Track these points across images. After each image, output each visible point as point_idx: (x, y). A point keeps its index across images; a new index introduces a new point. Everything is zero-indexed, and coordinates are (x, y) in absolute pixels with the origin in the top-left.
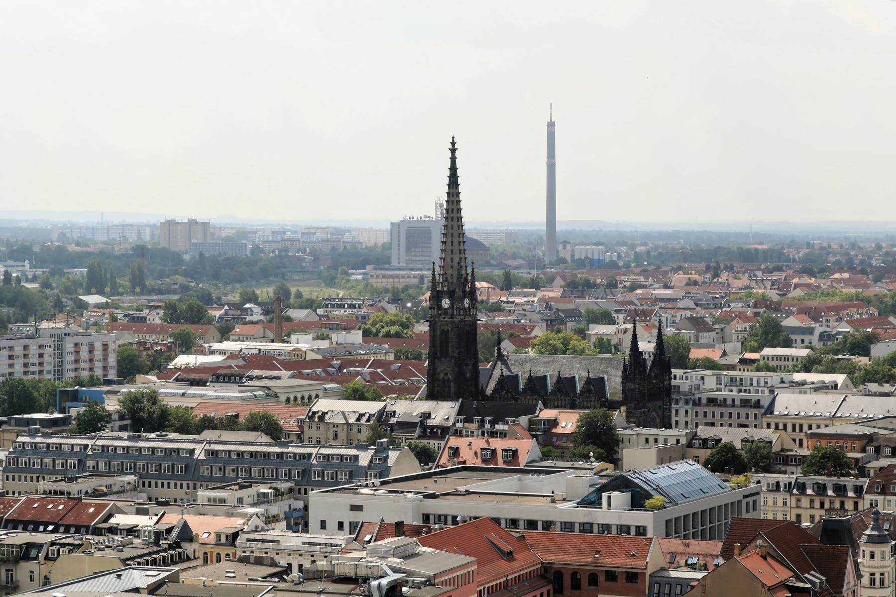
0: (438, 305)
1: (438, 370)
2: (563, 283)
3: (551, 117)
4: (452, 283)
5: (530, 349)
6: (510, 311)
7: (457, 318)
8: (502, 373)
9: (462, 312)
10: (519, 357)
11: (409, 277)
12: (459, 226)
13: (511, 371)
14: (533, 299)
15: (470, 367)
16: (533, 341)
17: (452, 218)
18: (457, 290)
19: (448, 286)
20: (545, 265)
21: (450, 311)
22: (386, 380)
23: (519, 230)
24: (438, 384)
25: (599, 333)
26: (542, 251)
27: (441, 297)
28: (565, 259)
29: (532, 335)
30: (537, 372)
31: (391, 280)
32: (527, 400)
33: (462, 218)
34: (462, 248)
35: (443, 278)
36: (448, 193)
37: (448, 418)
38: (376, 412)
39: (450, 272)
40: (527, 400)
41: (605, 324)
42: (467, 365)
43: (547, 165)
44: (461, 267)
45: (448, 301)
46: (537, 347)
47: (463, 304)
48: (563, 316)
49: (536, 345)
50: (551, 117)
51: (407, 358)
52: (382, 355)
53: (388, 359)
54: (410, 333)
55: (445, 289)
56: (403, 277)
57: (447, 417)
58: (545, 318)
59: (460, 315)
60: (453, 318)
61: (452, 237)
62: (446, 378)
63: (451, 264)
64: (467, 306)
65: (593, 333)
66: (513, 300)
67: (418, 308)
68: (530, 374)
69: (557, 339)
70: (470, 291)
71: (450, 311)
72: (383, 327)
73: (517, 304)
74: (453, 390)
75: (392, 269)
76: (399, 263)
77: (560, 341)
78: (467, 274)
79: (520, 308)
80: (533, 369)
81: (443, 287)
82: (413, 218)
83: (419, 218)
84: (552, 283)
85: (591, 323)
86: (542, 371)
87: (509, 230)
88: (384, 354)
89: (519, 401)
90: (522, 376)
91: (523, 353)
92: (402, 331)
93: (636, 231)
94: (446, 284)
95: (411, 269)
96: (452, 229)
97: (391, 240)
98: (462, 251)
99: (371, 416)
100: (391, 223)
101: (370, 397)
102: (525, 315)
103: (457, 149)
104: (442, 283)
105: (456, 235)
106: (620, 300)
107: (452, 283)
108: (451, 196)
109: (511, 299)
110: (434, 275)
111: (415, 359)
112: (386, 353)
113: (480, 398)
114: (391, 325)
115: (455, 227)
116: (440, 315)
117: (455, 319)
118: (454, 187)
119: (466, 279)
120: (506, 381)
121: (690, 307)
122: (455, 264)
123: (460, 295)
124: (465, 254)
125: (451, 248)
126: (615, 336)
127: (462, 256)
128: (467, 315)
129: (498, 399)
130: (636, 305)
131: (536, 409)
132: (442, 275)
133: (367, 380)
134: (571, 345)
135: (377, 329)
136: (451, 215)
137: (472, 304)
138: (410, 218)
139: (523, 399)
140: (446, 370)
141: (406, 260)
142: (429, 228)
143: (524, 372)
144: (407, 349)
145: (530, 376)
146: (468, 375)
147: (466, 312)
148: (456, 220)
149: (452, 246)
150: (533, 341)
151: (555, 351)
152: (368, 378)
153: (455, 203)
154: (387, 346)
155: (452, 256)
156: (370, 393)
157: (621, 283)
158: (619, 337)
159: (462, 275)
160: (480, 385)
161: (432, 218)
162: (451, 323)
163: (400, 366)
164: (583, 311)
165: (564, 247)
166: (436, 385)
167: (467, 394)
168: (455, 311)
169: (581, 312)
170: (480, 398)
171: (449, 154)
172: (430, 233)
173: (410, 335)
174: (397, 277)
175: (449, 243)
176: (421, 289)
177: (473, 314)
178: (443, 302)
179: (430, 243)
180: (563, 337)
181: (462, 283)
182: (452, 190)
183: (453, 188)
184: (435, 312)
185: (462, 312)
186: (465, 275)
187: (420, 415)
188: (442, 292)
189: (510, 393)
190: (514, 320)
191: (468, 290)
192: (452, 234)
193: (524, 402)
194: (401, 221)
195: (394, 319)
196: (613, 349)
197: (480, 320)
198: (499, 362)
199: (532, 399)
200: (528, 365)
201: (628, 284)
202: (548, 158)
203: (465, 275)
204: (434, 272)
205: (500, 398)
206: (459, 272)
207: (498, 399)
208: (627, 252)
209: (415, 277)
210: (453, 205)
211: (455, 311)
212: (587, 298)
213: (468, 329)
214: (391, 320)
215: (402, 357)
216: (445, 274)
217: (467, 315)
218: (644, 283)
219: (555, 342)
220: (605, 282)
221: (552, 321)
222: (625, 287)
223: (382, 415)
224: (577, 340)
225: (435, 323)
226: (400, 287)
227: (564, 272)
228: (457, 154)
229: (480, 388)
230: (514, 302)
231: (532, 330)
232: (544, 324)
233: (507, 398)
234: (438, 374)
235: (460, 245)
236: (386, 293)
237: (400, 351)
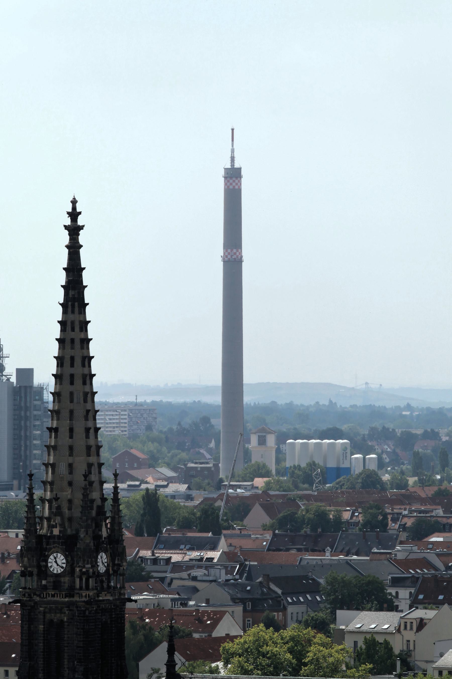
0: (39, 567)
2: (267, 520)
3: (233, 159)
4: (70, 519)
5: (220, 664)
7: (81, 596)
9: (91, 582)
16: (228, 645)
17: (72, 376)
19: (62, 525)
20: (221, 481)
21: (66, 579)
23: (153, 402)
25: (364, 629)
27: (46, 550)
28: (264, 466)
29: (219, 632)
34: (92, 442)
39: (67, 494)
41: (370, 610)
43: (224, 262)
44: (91, 483)
45: (61, 559)
47: (95, 565)
48: (279, 591)
49: (233, 655)
50: (233, 159)
55: (56, 531)
58: (239, 596)
59: (87, 588)
60: (73, 596)
61: (71, 419)
64: (102, 569)
65: (351, 627)
70: (109, 537)
73: (178, 567)
77: (286, 647)
78: (104, 500)
79: (184, 575)
81: (51, 527)
85: (342, 608)
93: (408, 407)
96: (72, 401)
98: (93, 449)
102: (195, 590)
103: (82, 227)
104: (49, 519)
105: (79, 413)
106: (400, 556)
107: (70, 519)
108: (69, 328)
109: (162, 554)
115: (79, 397)
116: (45, 588)
117: (76, 598)
118: (77, 309)
119: (101, 511)
122: (78, 478)
126: (398, 636)
127: (92, 459)
128: (102, 589)
130: (436, 569)
132: (50, 501)
134: (310, 654)
136: (68, 370)
137: (114, 565)
147: (102, 582)
148: (81, 382)
149: (71, 437)
153: (77, 344)
155: (70, 460)
157: (394, 520)
158: (406, 638)
159: (92, 501)
162: (69, 605)
164: (322, 581)
165: (262, 441)
168: (78, 581)
169: (319, 584)
171: (65, 238)
177: (115, 588)
180: (292, 639)
182: (71, 317)
183: (73, 312)
184: (32, 583)
185: (91, 582)
186: (99, 502)
188: (49, 538)
190: (173, 600)
191: (104, 533)
192: (71, 412)
196: (398, 664)
201: (409, 522)
203: (99, 502)
206: (85, 496)
208: (394, 452)
210: (72, 348)
211: (78, 581)
212: (328, 554)
216: (57, 499)
217: (102, 588)
218: (445, 521)
220: (361, 518)
221: (254, 602)
222: (404, 527)
224: (323, 645)
227: (269, 495)
228: (83, 238)
232: (239, 609)
235: (87, 437)
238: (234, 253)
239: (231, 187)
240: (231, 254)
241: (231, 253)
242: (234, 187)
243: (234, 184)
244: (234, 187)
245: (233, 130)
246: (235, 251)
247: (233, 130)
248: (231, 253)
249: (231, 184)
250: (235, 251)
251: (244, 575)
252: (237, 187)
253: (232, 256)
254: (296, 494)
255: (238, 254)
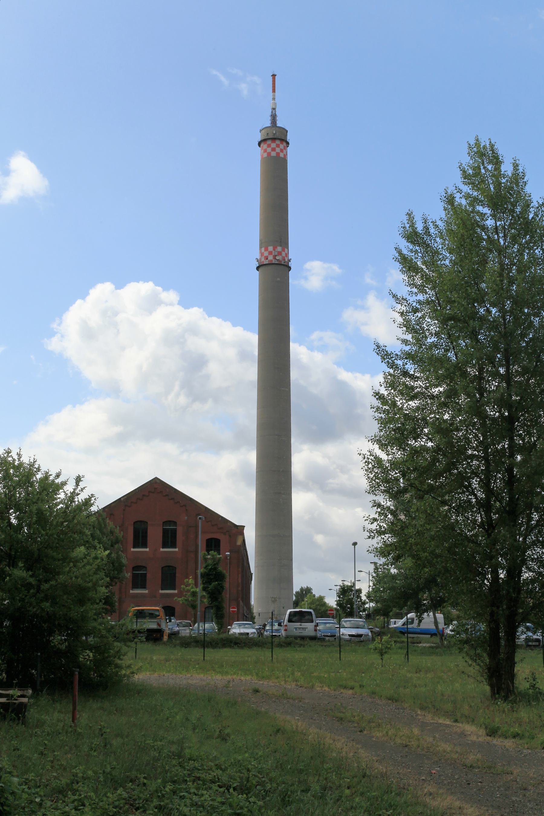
3: (274, 118)
238: (275, 148)
239: (273, 154)
240: (273, 254)
241: (273, 251)
242: (278, 154)
243: (278, 150)
244: (278, 154)
245: (274, 76)
246: (279, 249)
247: (274, 76)
248: (273, 251)
251: (132, 593)
252: (282, 155)
253: (275, 257)
254: (227, 673)
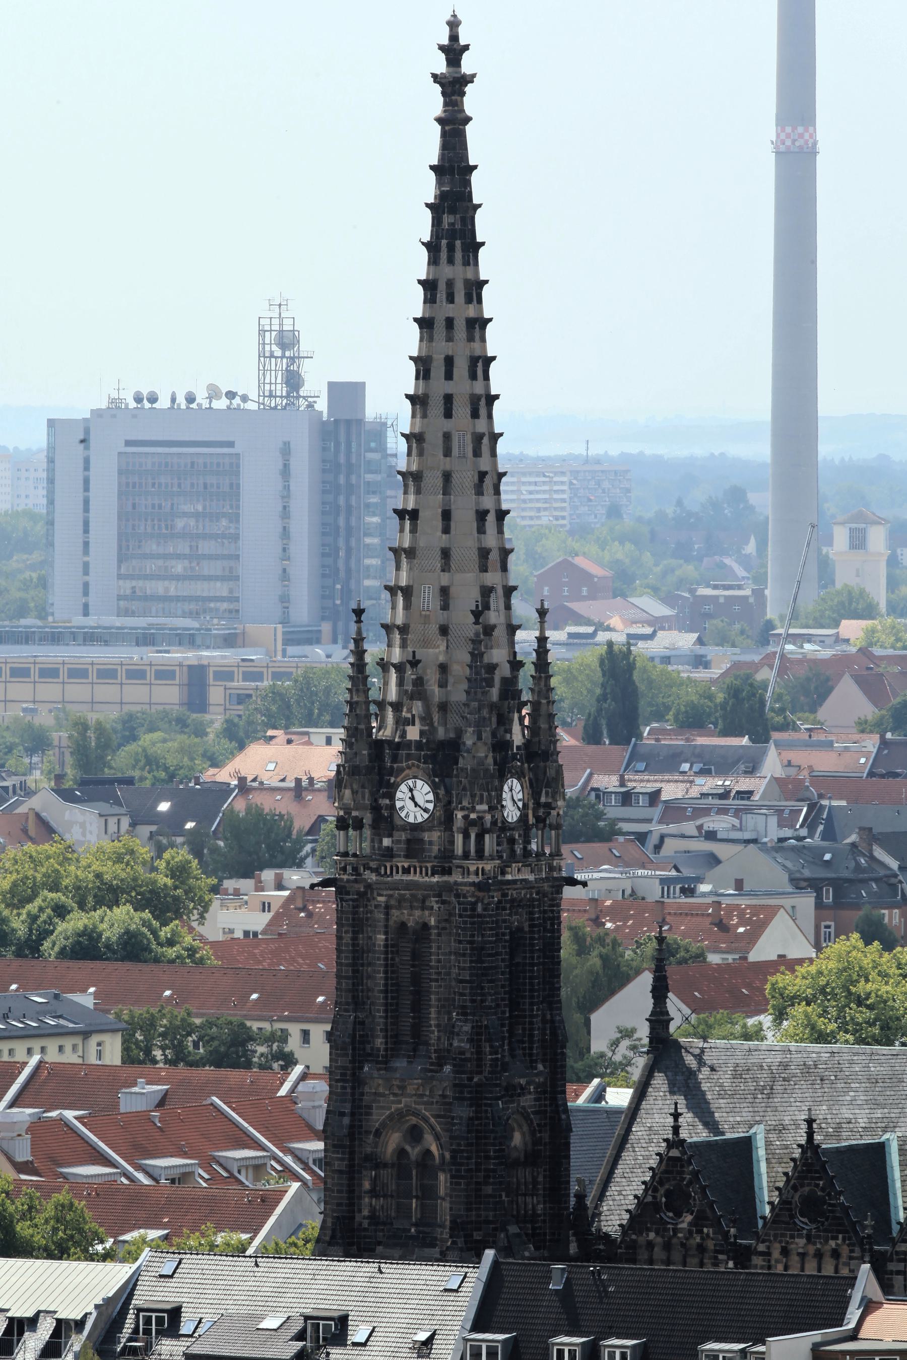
0: (376, 809)
1: (378, 1117)
2: (868, 710)
4: (444, 707)
5: (766, 1020)
6: (642, 837)
7: (466, 872)
8: (676, 1129)
10: (754, 1059)
11: (136, 674)
12: (478, 439)
13: (711, 1125)
14: (744, 784)
15: (527, 1101)
16: (782, 979)
17: (448, 399)
18: (469, 740)
19: (426, 719)
20: (770, 625)
21: (434, 837)
22: (107, 1161)
24: (374, 1181)
26: (745, 562)
27: (391, 772)
30: (838, 1128)
31: (50, 690)
32: (795, 1260)
33: (491, 399)
34: (490, 540)
35: (401, 683)
36: (429, 285)
37: (428, 1342)
38: (90, 1308)
39: (435, 653)
40: (795, 1260)
42: (512, 1092)
44: (489, 630)
45: (424, 792)
46: (799, 1010)
47: (496, 805)
49: (794, 999)
51: (179, 1057)
52: (68, 1043)
53: (93, 1060)
54: (188, 940)
56: (107, 674)
57: (423, 1336)
58: (807, 873)
59: (480, 855)
60: (449, 873)
61: (446, 491)
62: (414, 1152)
63: (441, 617)
66: (650, 787)
67: (204, 819)
68: (810, 1134)
69: (894, 971)
70: (527, 744)
71: (434, 837)
72: (61, 911)
74: (444, 1210)
75: (55, 638)
76: (86, 614)
78: (516, 665)
79: (689, 827)
80: (821, 1112)
81: (402, 723)
82: (153, 399)
83: (181, 401)
84: (813, 710)
86: (862, 1122)
87: (587, 460)
88: (78, 1040)
89: (757, 1261)
90: (768, 1143)
91: (732, 1036)
92: (154, 933)
94: (418, 707)
95: (146, 639)
96: (447, 453)
97: (51, 502)
98: (494, 556)
99: (63, 1328)
100: (51, 423)
101: (39, 1240)
102: (714, 860)
104: (397, 707)
105: (465, 477)
107: (444, 707)
108: (441, 295)
109: (642, 784)
110: (359, 666)
111: (219, 1060)
112: (86, 1035)
113: (573, 1249)
114: (100, 902)
115: (462, 443)
116: (389, 854)
117: (456, 877)
118: (458, 255)
119: (510, 689)
120: (694, 1167)
121: (687, 834)
123: (481, 762)
124: (504, 568)
125: (442, 540)
127: (492, 578)
129: (658, 1253)
131: (846, 1301)
132: (400, 668)
133: (20, 1159)
135: (33, 918)
136: (439, 386)
137: (538, 804)
138: (138, 399)
139: (776, 1254)
140: (416, 1114)
141: (120, 598)
142: (231, 444)
143: (781, 1129)
144: (181, 1013)
145: (810, 1146)
146: (517, 1139)
149: (446, 530)
150: (782, 979)
151: (885, 1027)
152: (24, 1154)
154: (87, 999)
155: (445, 579)
156: (39, 1219)
160: (574, 1188)
161: (245, 398)
162: (441, 891)
163: (167, 1092)
166: (367, 1185)
167: (513, 1229)
168: (459, 839)
170: (573, 1249)
171: (435, 102)
172: (233, 468)
173: (192, 951)
174: (77, 673)
175: (431, 518)
176: (200, 731)
178: (402, 792)
179: (235, 518)
181: (492, 707)
182: (447, 271)
183: (451, 261)
187: (297, 1326)
188: (398, 747)
189: (716, 1223)
191: (517, 737)
192: (447, 477)
193: (780, 1269)
194: (97, 414)
195: (112, 872)
197: (573, 882)
198: (660, 1081)
199: (819, 1255)
200: (798, 1095)
202: (781, 121)
203: (505, 670)
204: (359, 653)
205: (667, 1246)
206: (476, 655)
207: (658, 1253)
209: (165, 675)
210: (450, 339)
211: (459, 839)
213: (515, 921)
214: (98, 876)
215: (158, 1054)
216: (415, 663)
219: (885, 989)
223: (117, 1323)
225: (362, 895)
226: (110, 715)
229: (573, 1201)
230: (654, 797)
231: (757, 929)
232: (806, 902)
233: (701, 1248)
234: (378, 1133)
235: (481, 530)
236: (31, 751)
237: (149, 1025)
246: (800, 129)
249: (801, 136)
250: (800, 129)
253: (794, 141)
255: (807, 136)
